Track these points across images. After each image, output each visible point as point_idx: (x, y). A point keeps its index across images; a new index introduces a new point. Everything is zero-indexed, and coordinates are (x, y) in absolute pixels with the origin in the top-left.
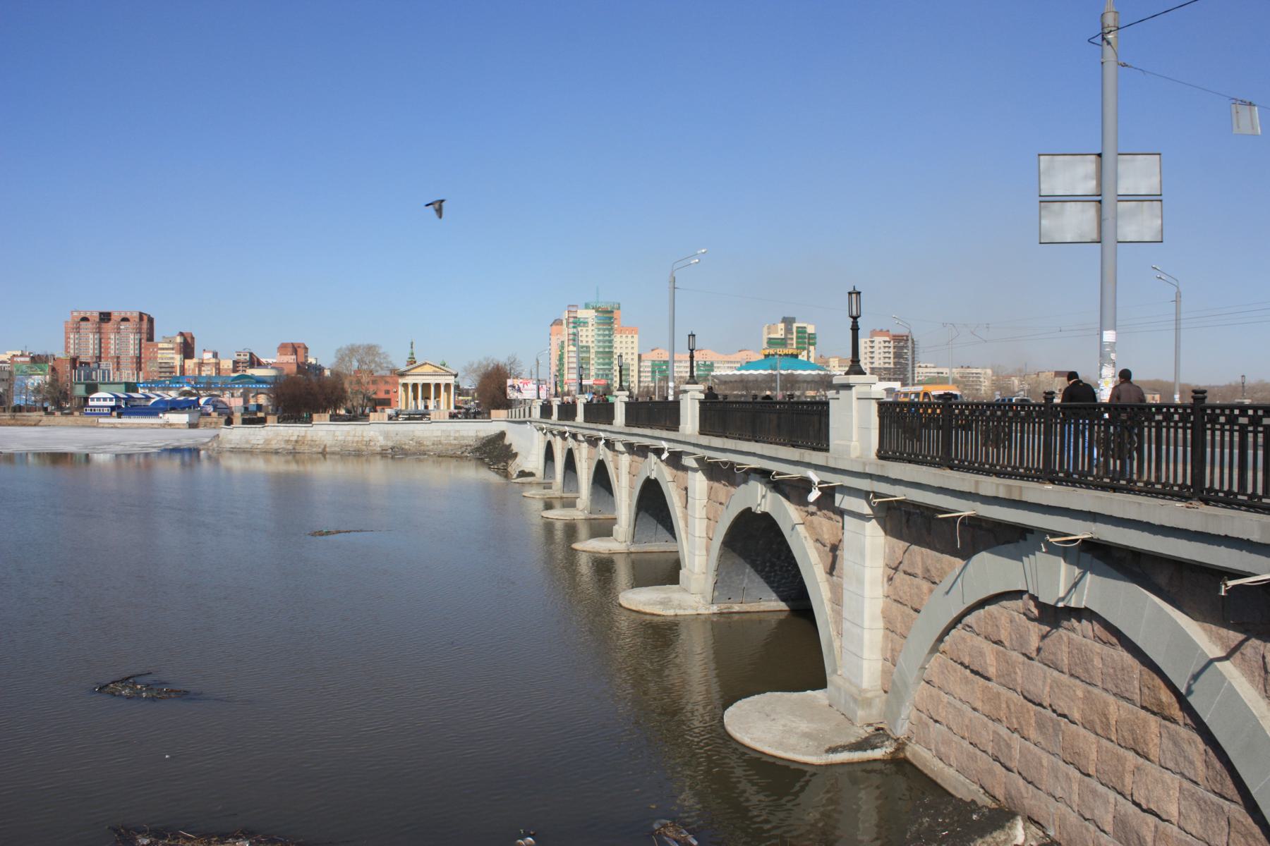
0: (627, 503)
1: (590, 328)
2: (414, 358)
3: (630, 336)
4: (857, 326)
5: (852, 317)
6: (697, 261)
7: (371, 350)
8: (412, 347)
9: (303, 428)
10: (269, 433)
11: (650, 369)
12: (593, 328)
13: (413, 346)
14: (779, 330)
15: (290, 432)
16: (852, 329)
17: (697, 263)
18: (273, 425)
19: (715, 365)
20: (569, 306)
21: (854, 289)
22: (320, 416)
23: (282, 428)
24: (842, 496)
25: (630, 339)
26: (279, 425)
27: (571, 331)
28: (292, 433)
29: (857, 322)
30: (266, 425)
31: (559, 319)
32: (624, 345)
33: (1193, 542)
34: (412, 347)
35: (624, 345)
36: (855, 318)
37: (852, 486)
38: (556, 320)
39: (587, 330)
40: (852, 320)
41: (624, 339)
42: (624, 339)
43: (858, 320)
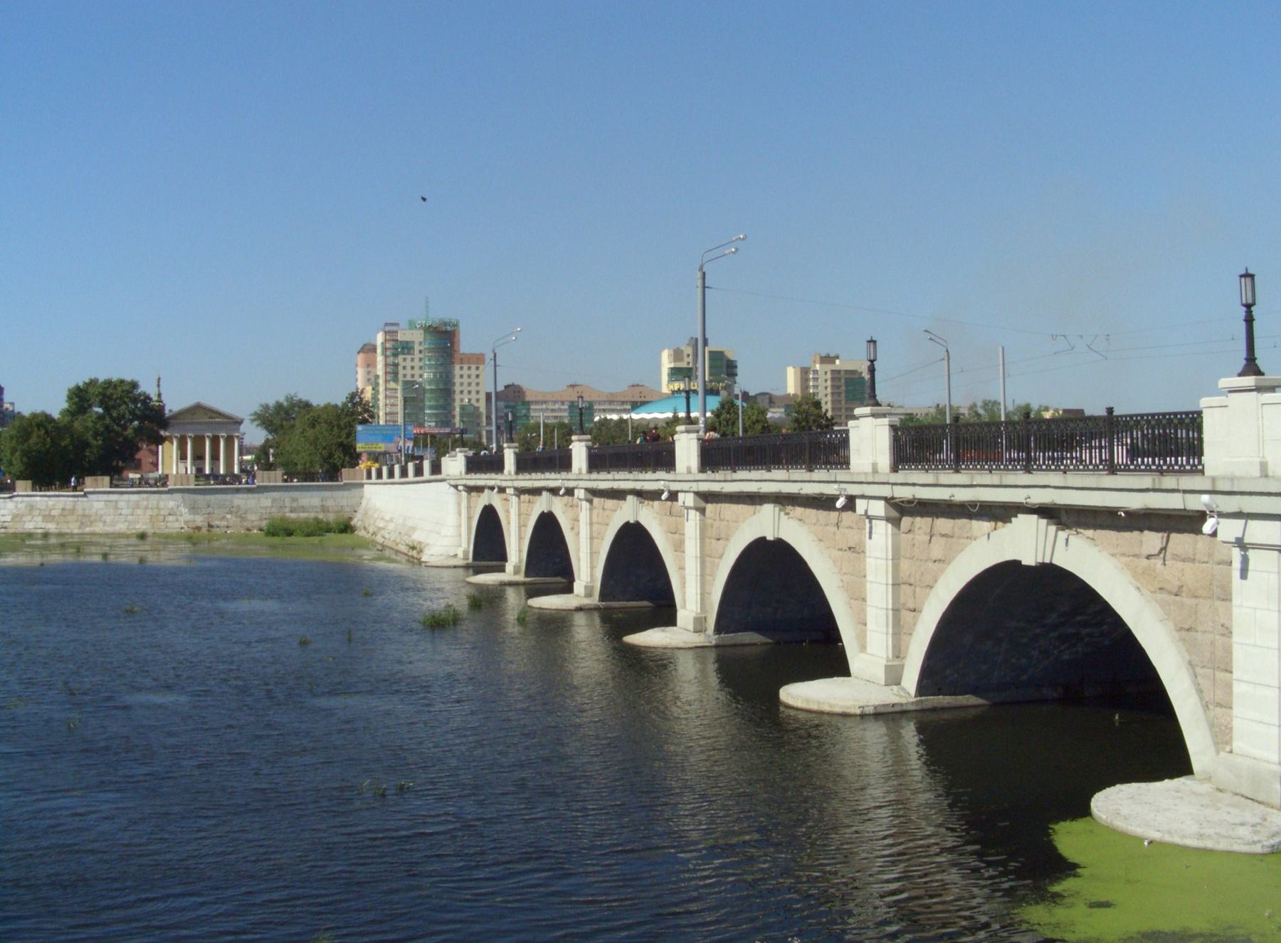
0: (687, 571)
1: (417, 356)
2: (162, 402)
3: (466, 367)
4: (1252, 316)
5: (1244, 305)
6: (733, 250)
7: (70, 390)
8: (159, 386)
9: (70, 499)
10: (20, 506)
11: (532, 407)
12: (422, 356)
13: (161, 383)
14: (685, 356)
15: (50, 503)
16: (1246, 320)
17: (732, 252)
18: (26, 493)
19: (595, 407)
20: (386, 324)
21: (1247, 270)
22: (96, 480)
23: (38, 499)
24: (1244, 521)
25: (473, 372)
26: (34, 493)
27: (391, 360)
28: (53, 505)
29: (1251, 312)
30: (15, 493)
31: (369, 344)
32: (465, 380)
33: (835, 678)
34: (159, 386)
35: (465, 380)
36: (1248, 307)
37: (1264, 512)
38: (365, 345)
39: (412, 360)
40: (1245, 309)
41: (465, 372)
42: (465, 372)
43: (1253, 309)
